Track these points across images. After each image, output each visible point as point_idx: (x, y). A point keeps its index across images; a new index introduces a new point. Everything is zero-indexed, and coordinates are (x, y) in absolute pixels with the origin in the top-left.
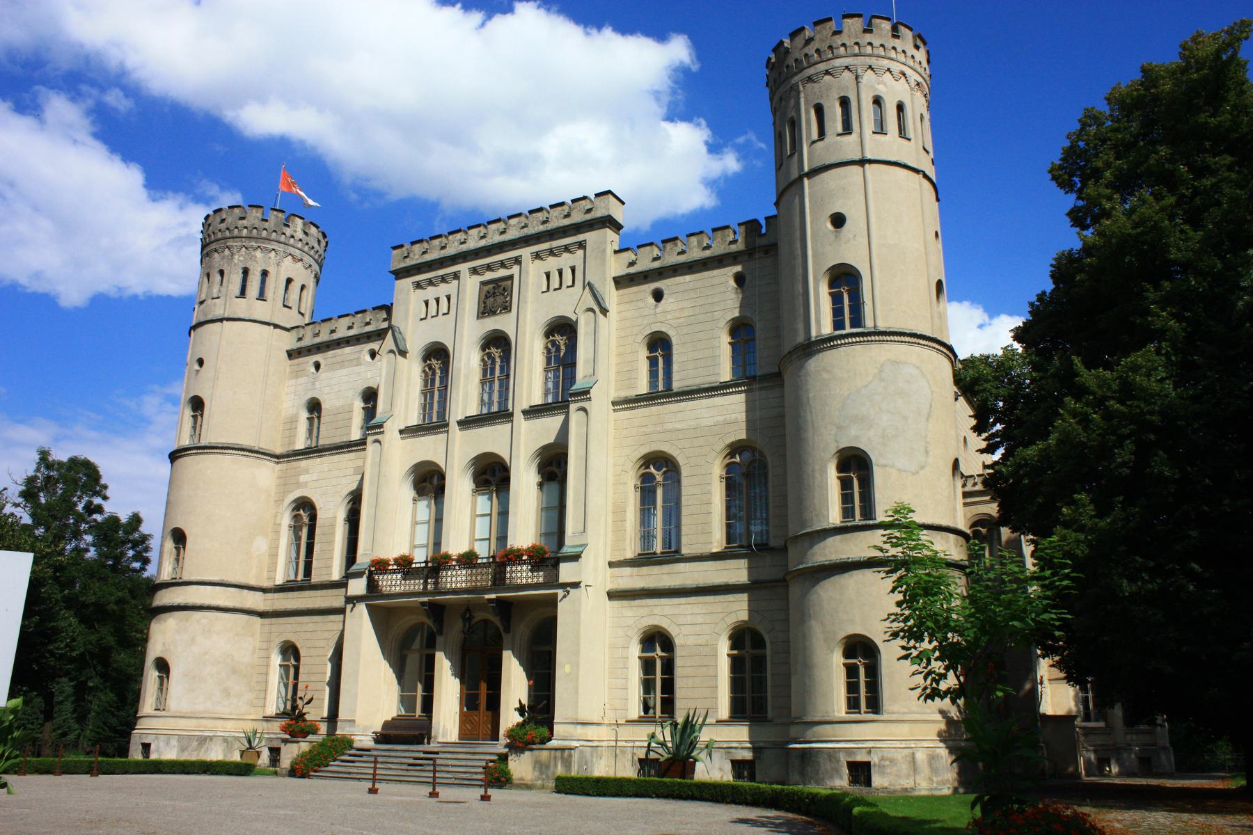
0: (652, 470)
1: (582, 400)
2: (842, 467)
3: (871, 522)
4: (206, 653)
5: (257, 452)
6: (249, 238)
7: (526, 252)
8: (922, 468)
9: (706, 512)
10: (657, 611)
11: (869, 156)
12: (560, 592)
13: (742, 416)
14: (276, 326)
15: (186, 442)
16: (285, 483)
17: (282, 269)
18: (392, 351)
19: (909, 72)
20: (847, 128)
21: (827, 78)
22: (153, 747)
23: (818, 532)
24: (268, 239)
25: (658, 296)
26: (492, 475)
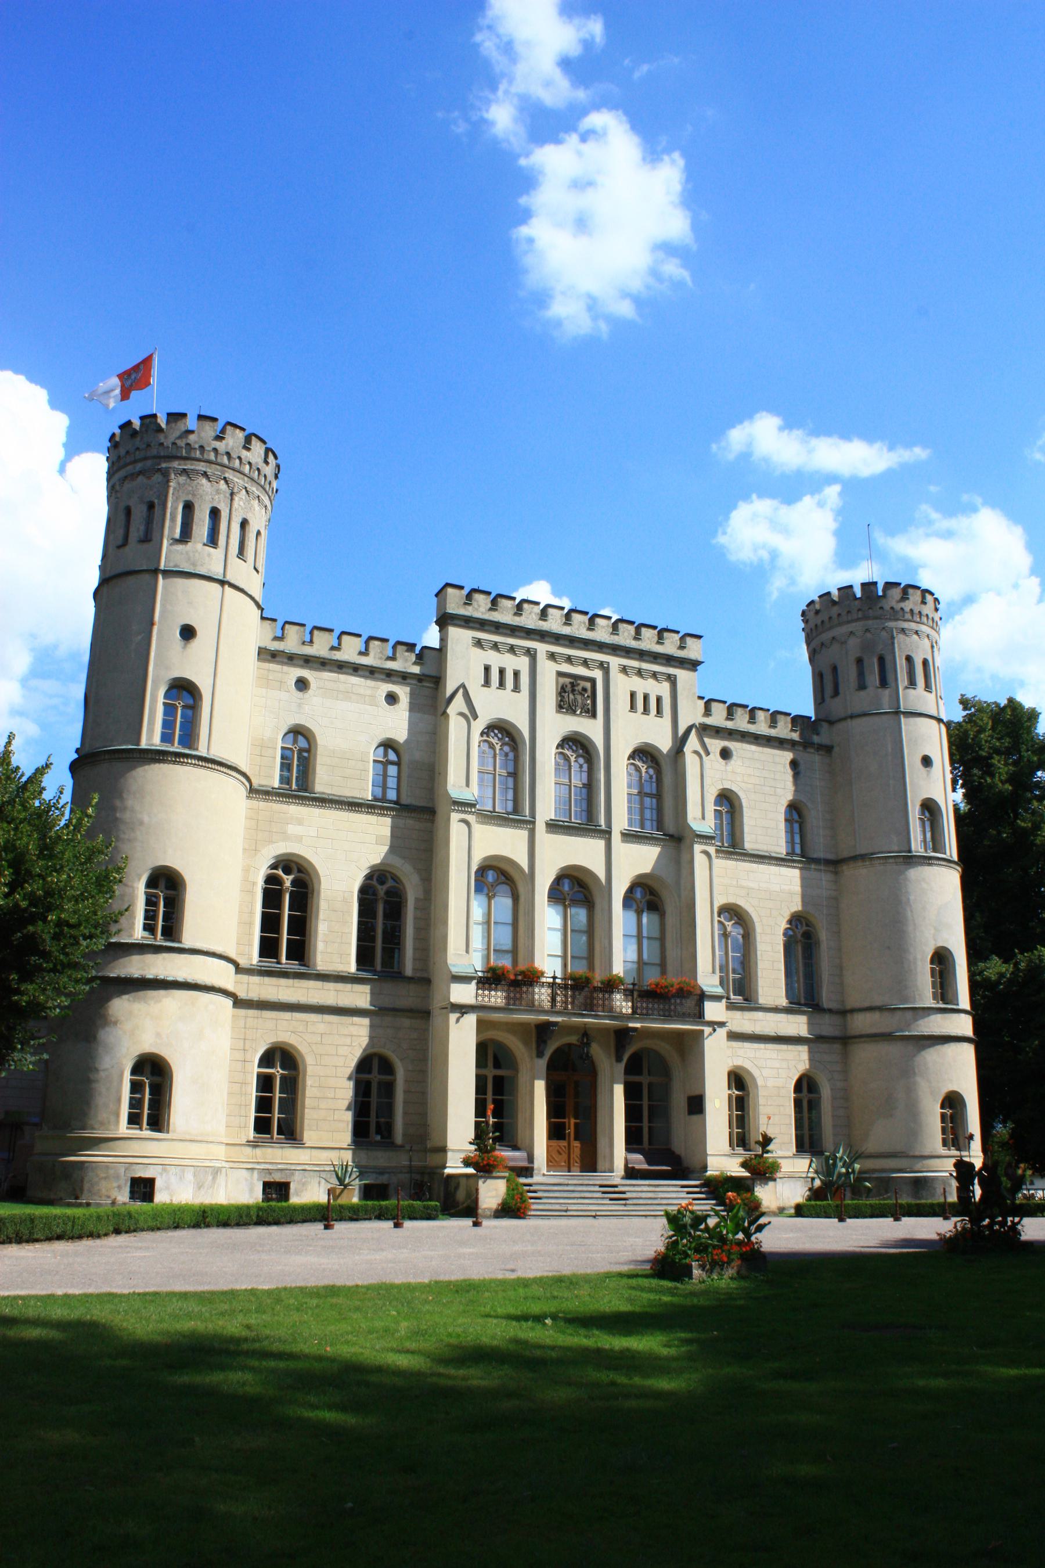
0: (280, 872)
1: (706, 844)
2: (152, 883)
3: (176, 945)
10: (741, 1052)
11: (229, 578)
12: (707, 1030)
13: (798, 889)
18: (462, 714)
20: (213, 540)
21: (915, 637)
22: (158, 1184)
23: (923, 1008)
26: (576, 889)
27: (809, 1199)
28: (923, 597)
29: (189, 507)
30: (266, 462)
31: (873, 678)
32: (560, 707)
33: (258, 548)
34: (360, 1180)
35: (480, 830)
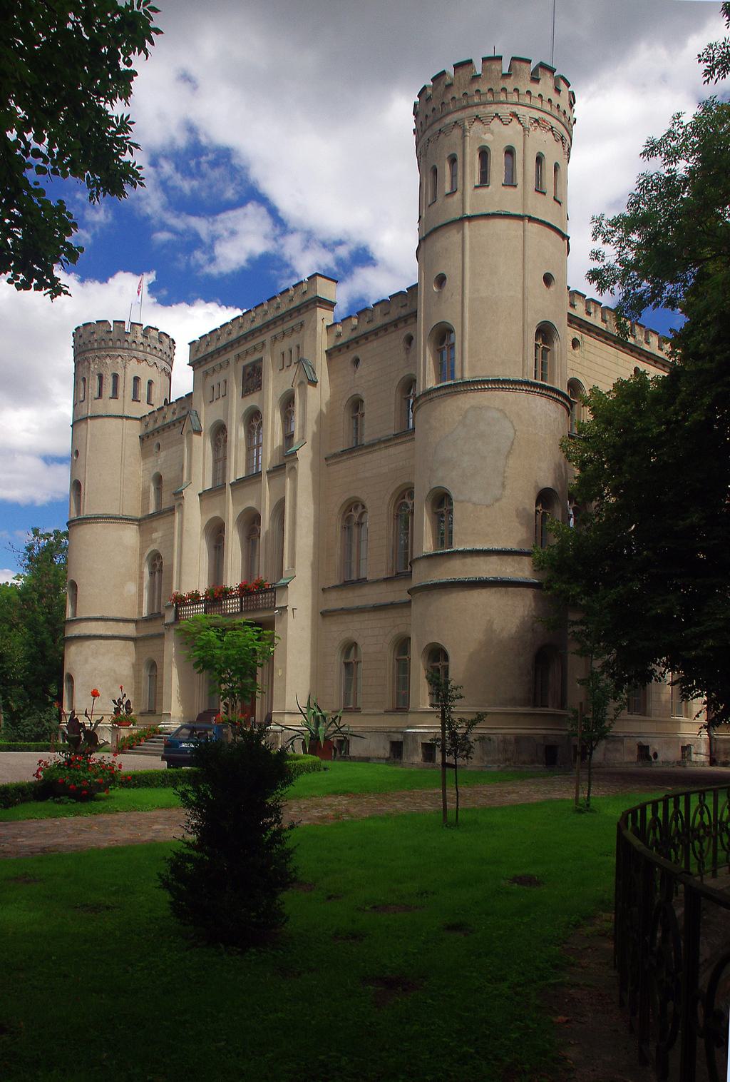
4: (95, 669)
5: (121, 519)
6: (100, 349)
7: (267, 337)
8: (497, 500)
14: (128, 418)
15: (74, 516)
16: (143, 544)
17: (128, 371)
19: (521, 111)
20: (115, 395)
24: (115, 348)
25: (356, 362)
27: (75, 724)
30: (558, 91)
34: (165, 753)
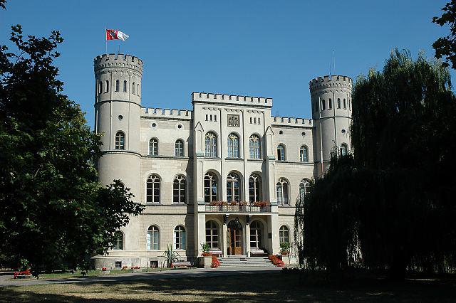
9: (167, 194)
28: (344, 79)
29: (324, 101)
31: (121, 88)
32: (229, 125)
33: (138, 90)
35: (205, 162)
